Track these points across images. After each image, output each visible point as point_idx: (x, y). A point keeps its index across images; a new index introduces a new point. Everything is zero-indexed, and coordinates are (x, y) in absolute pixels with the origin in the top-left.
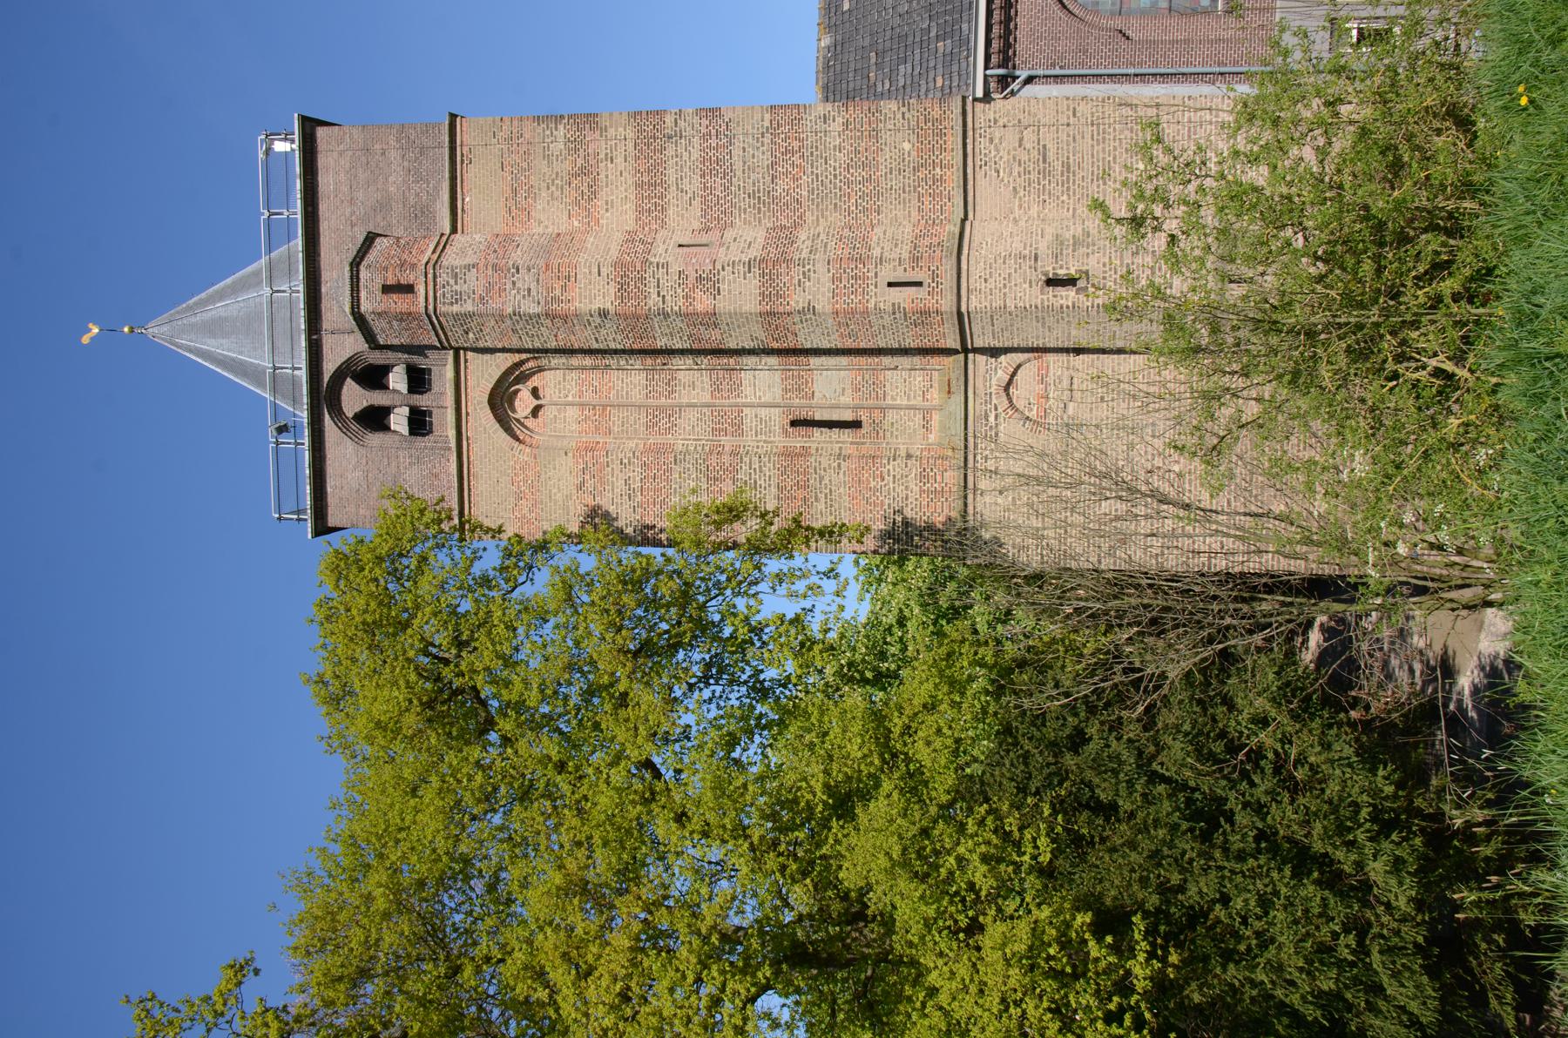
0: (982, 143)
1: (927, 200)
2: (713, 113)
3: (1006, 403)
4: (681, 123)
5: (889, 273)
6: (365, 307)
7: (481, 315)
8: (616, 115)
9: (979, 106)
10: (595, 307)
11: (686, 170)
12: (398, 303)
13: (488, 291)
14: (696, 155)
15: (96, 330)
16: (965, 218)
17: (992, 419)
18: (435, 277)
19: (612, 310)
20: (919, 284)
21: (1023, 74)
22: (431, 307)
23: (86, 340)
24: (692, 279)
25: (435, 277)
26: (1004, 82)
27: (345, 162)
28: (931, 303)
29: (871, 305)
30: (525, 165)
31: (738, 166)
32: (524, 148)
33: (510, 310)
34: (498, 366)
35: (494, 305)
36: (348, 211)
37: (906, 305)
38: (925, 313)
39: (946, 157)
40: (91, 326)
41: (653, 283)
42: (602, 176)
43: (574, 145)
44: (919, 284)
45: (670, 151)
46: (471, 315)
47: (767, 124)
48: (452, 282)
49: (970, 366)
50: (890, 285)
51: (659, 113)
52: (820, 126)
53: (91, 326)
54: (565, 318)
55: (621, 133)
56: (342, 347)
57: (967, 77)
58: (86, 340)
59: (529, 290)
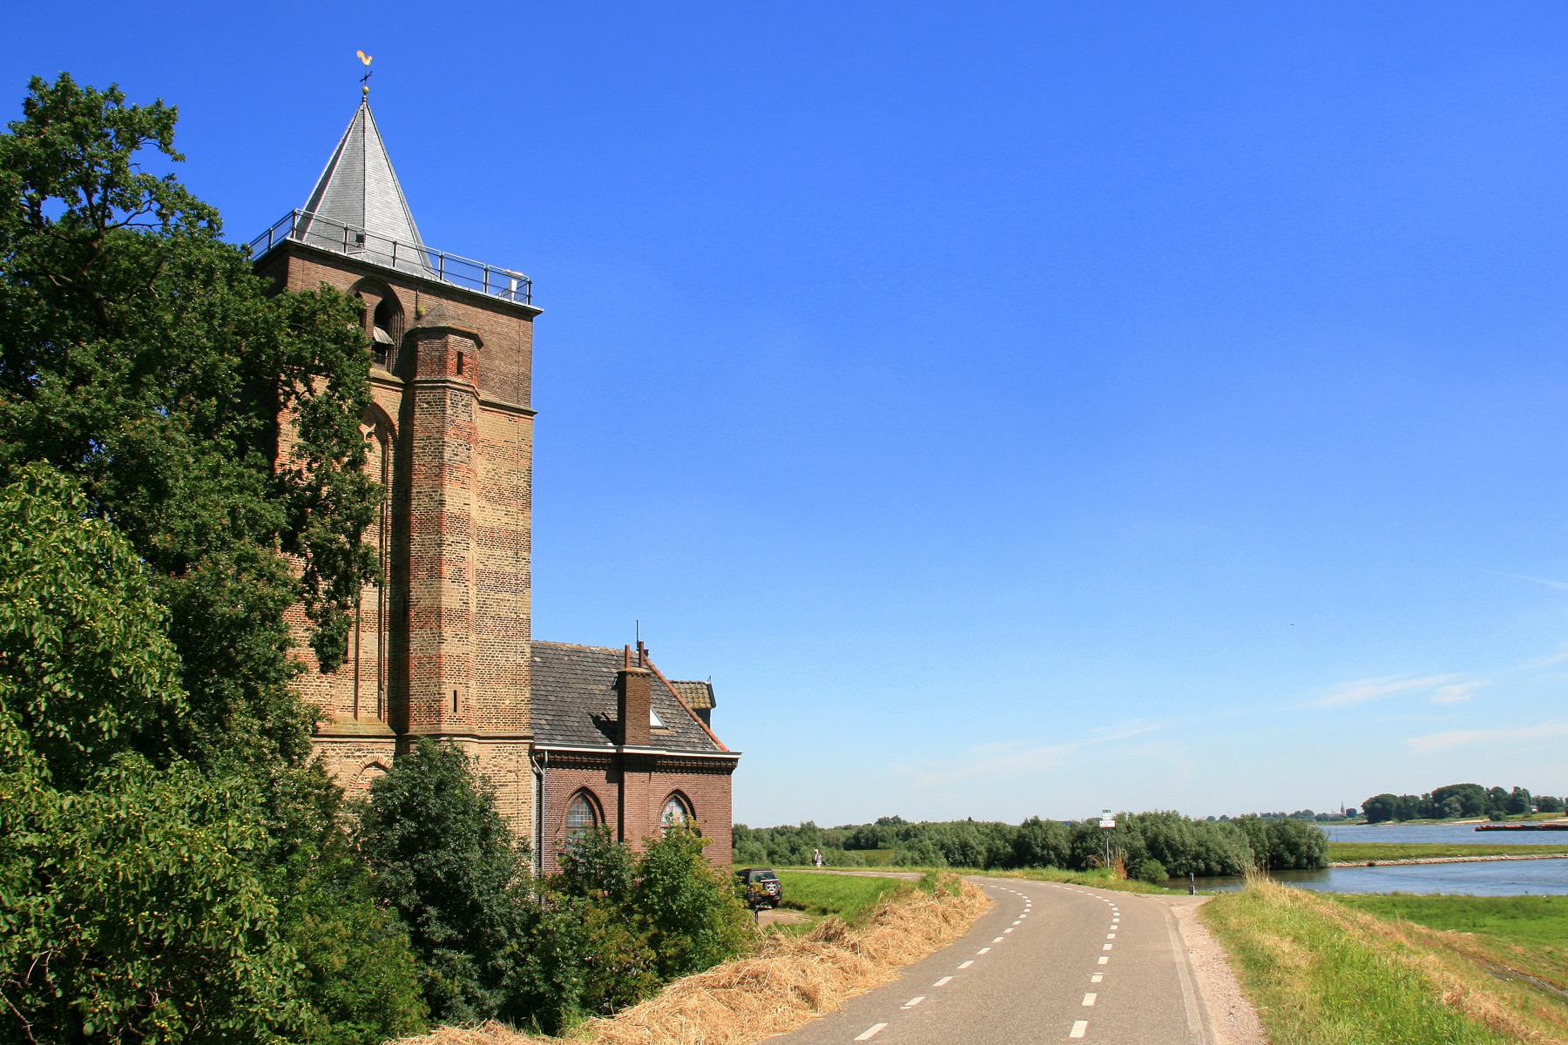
0: (509, 748)
1: (479, 713)
2: (528, 584)
3: (368, 763)
4: (523, 562)
5: (461, 690)
6: (452, 338)
7: (443, 418)
8: (529, 521)
9: (527, 746)
10: (447, 499)
11: (500, 562)
12: (452, 361)
13: (458, 426)
14: (507, 569)
15: (367, 62)
16: (479, 738)
17: (358, 753)
18: (467, 392)
19: (445, 509)
20: (455, 711)
21: (543, 772)
22: (449, 384)
23: (360, 54)
24: (461, 565)
25: (467, 392)
26: (541, 762)
27: (513, 334)
28: (445, 717)
29: (444, 680)
30: (506, 457)
31: (499, 596)
32: (515, 458)
33: (446, 440)
34: (393, 413)
35: (450, 430)
36: (487, 328)
37: (444, 703)
38: (439, 713)
39: (501, 726)
40: (370, 58)
41: (459, 539)
42: (499, 507)
43: (515, 491)
44: (455, 711)
45: (510, 553)
46: (444, 412)
47: (522, 616)
48: (463, 403)
49: (389, 740)
50: (455, 692)
51: (529, 550)
52: (520, 650)
53: (370, 58)
54: (440, 476)
55: (521, 522)
56: (405, 296)
57: (550, 737)
58: (360, 54)
59: (457, 455)
